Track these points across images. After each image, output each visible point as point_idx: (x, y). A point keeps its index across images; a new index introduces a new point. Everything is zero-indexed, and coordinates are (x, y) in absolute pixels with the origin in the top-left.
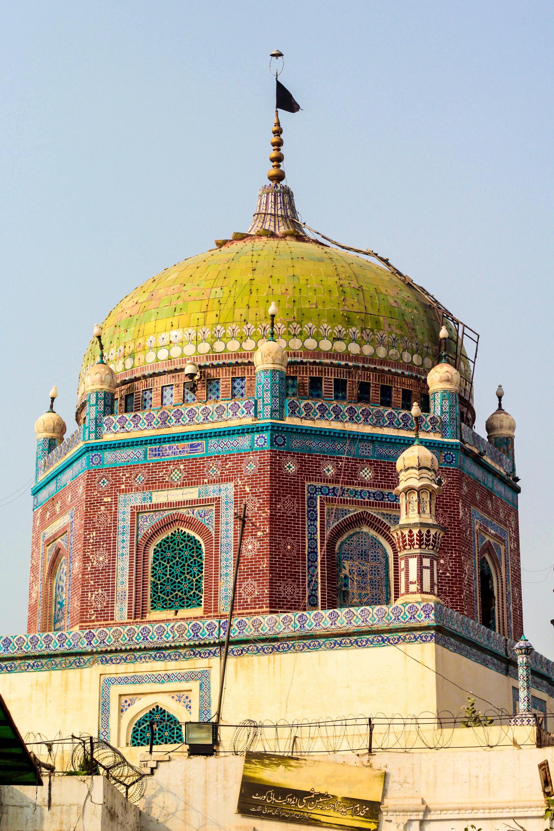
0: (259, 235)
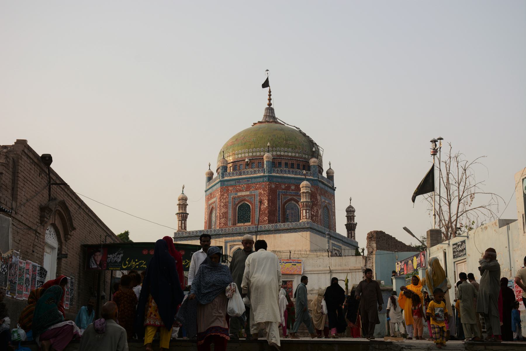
0: (265, 122)
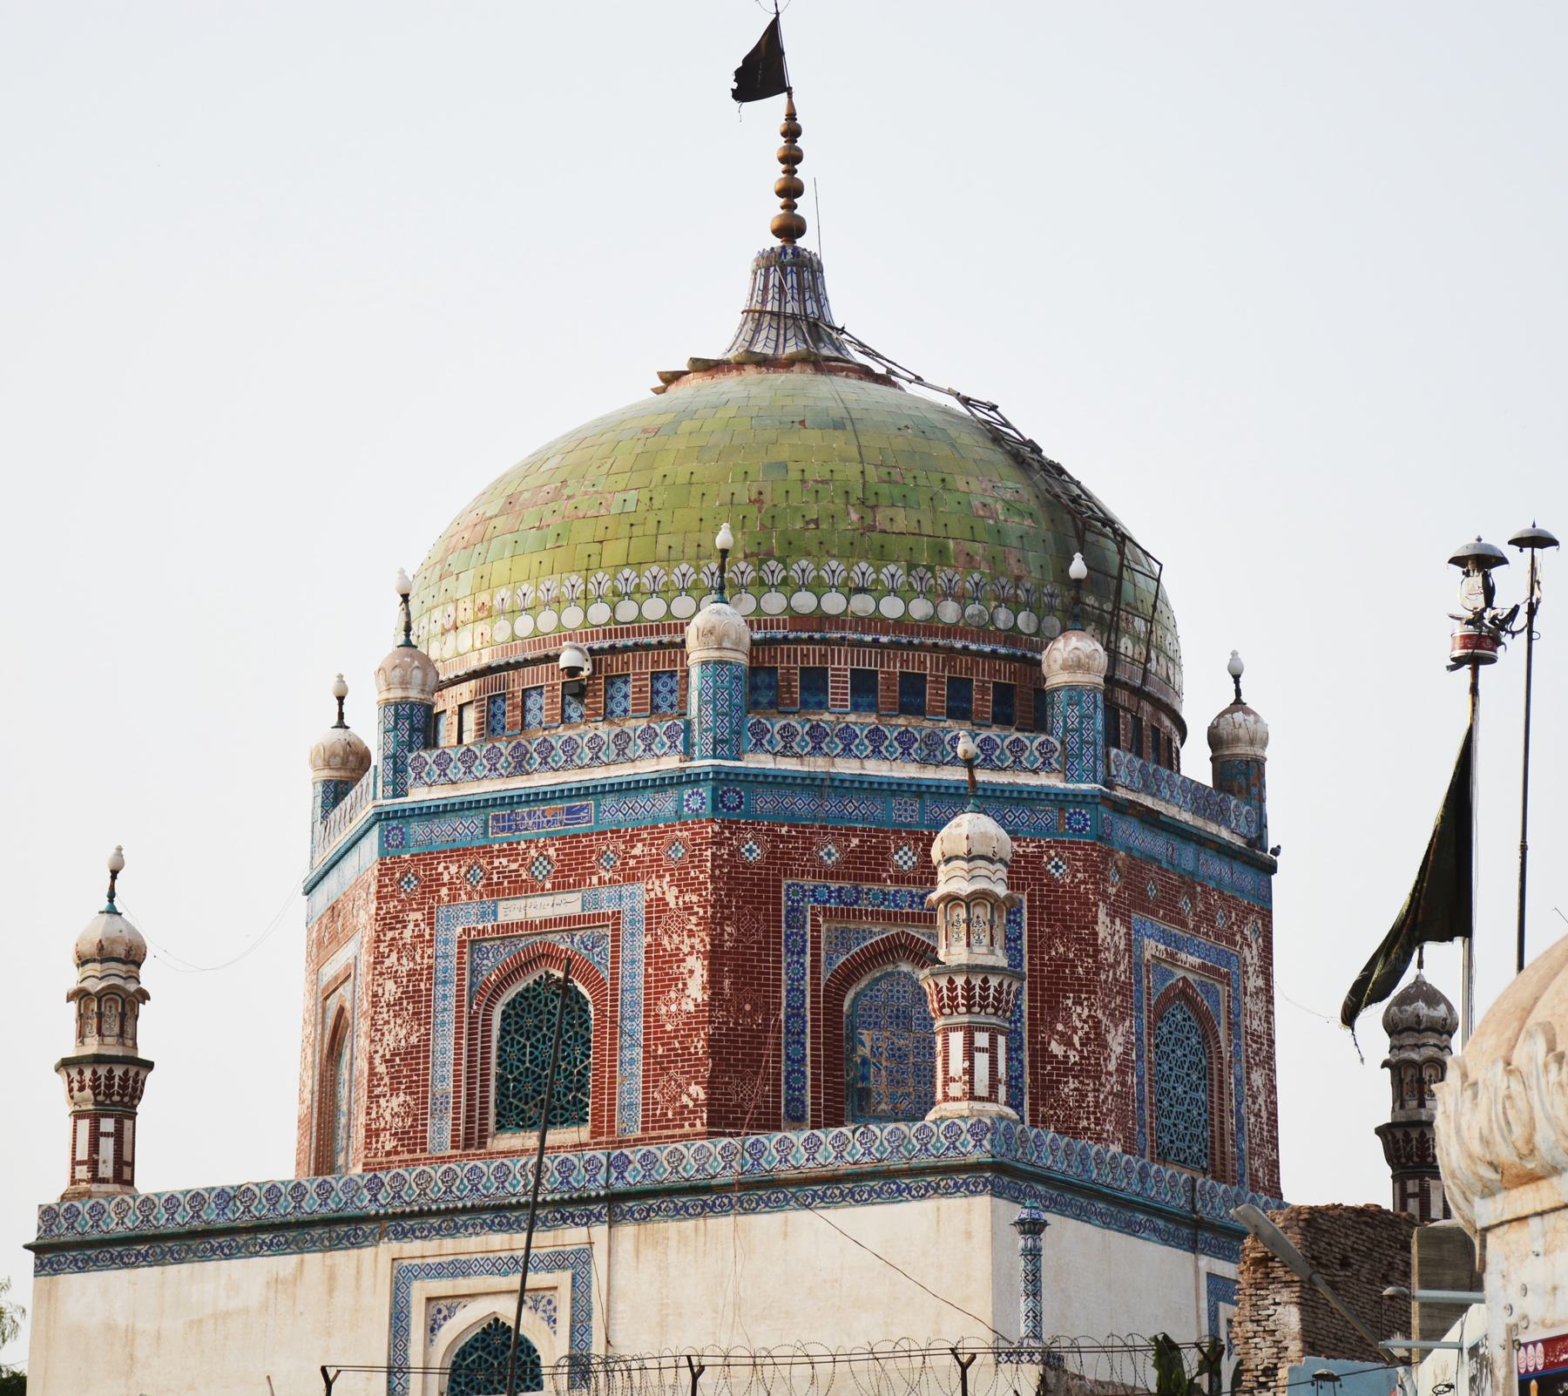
0: (739, 365)
